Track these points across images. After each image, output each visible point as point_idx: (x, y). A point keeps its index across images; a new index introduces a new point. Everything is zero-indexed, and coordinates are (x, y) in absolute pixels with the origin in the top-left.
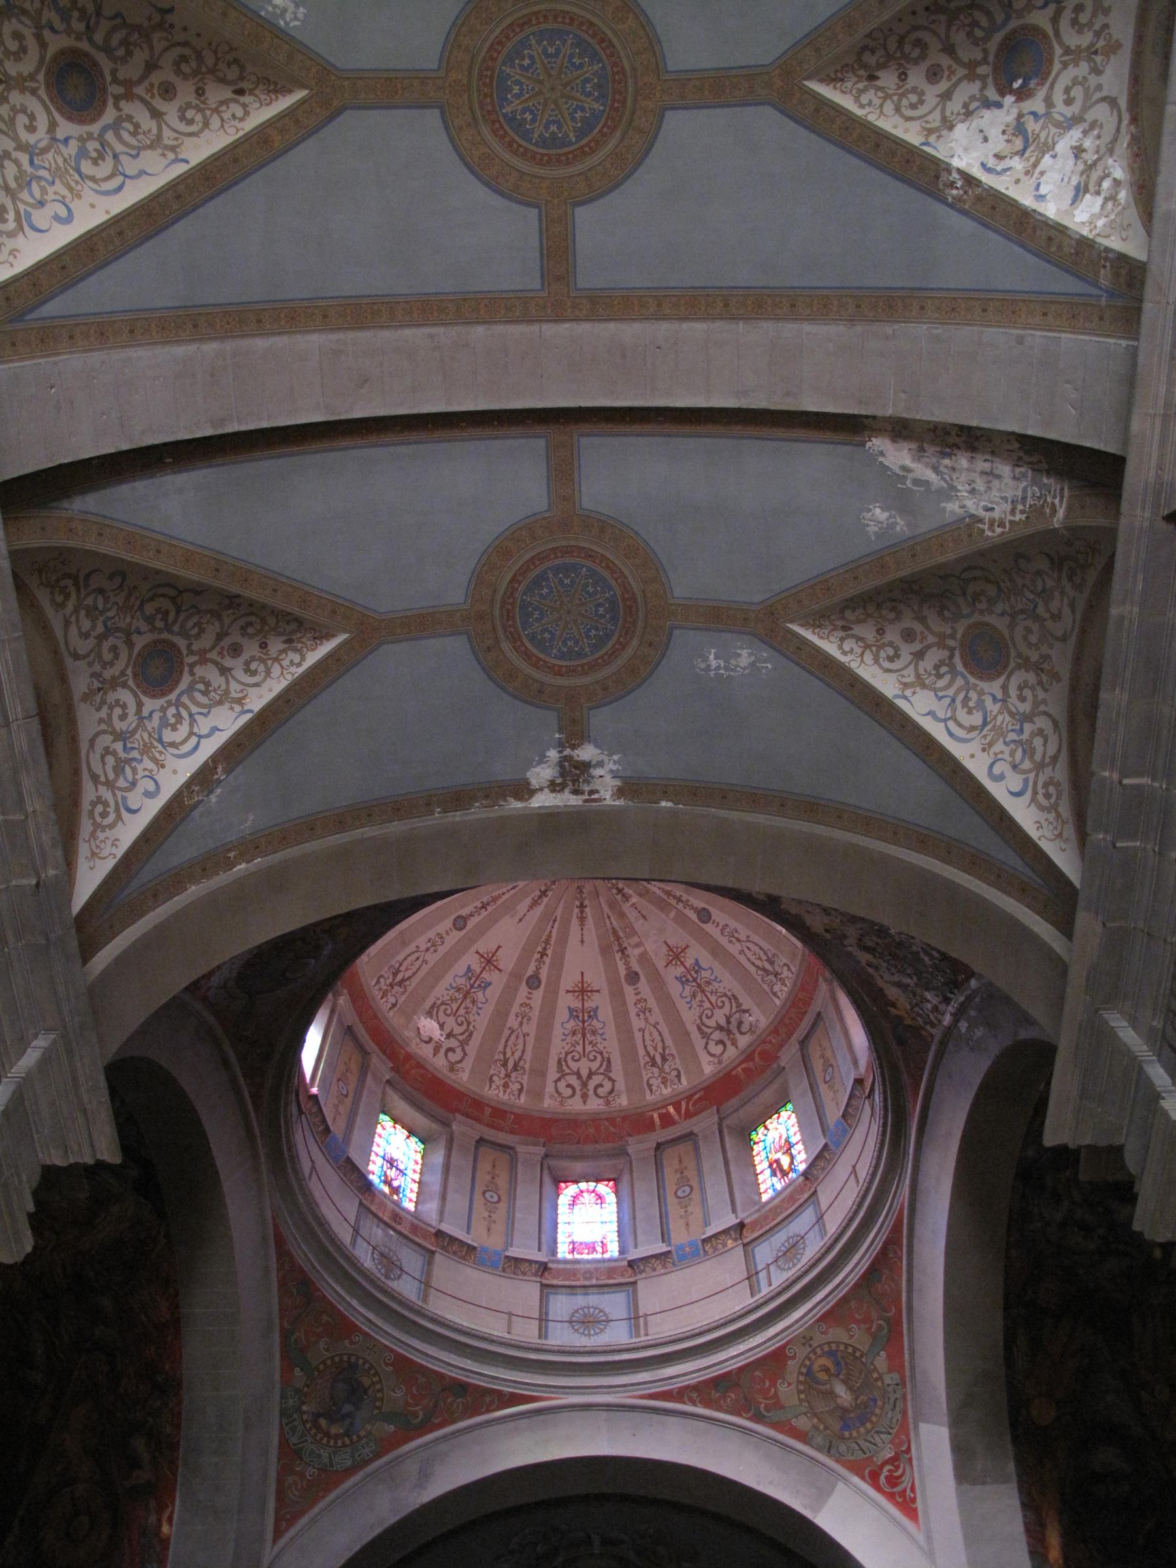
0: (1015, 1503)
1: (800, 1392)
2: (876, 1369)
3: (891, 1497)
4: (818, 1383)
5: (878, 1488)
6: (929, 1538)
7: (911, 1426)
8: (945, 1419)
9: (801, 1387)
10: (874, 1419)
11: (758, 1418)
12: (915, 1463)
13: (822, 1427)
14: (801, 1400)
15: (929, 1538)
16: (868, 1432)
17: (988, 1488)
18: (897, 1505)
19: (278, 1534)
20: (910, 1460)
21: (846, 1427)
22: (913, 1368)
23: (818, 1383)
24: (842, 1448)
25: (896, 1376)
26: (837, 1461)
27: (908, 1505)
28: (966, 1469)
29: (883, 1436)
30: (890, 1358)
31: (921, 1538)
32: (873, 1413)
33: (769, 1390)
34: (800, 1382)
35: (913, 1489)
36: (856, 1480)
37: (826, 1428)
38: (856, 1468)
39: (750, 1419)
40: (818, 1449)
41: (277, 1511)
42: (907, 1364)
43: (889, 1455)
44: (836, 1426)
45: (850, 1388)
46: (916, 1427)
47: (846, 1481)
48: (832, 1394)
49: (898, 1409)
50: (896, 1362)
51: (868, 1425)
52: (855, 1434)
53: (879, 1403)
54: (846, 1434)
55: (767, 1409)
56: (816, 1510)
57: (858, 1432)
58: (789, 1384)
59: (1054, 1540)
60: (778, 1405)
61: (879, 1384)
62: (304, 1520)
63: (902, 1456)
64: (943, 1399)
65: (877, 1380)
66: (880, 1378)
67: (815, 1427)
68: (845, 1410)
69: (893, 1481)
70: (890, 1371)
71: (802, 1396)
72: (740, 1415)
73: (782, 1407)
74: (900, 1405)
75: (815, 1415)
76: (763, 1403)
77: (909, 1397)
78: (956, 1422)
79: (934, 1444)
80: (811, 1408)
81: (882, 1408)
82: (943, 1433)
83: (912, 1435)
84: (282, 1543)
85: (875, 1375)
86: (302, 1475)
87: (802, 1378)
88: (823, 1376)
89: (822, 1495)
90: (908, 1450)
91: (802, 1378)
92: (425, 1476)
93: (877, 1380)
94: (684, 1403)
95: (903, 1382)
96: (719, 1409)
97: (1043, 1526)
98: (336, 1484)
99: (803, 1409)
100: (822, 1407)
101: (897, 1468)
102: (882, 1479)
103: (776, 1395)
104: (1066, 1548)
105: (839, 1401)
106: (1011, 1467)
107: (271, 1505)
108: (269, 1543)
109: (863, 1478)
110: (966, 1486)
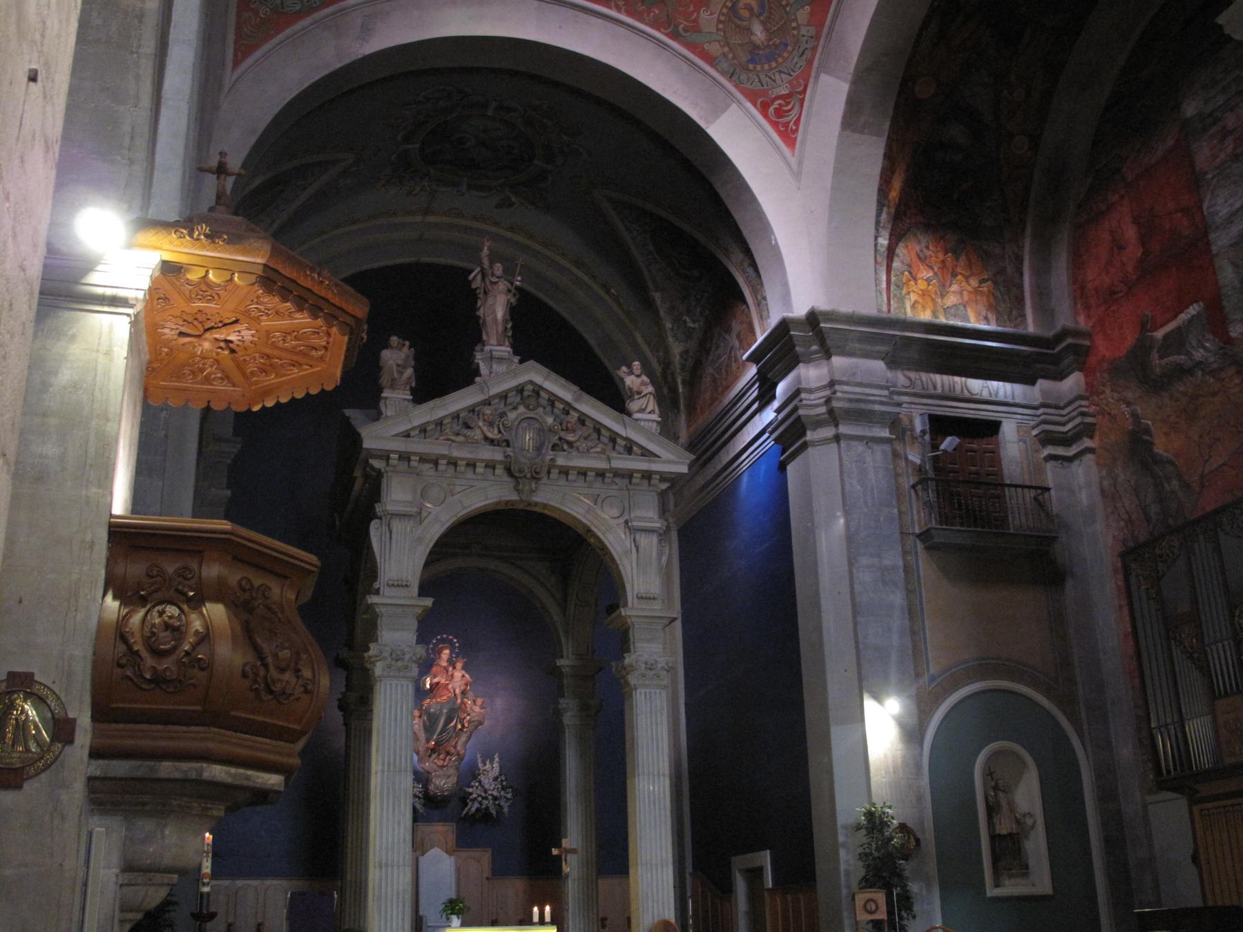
0: (881, 151)
1: (719, 21)
2: (796, 19)
3: (775, 125)
4: (741, 19)
5: (766, 116)
6: (800, 163)
7: (813, 74)
8: (850, 77)
9: (722, 18)
10: (780, 60)
11: (674, 36)
12: (806, 104)
13: (730, 56)
14: (718, 30)
15: (800, 163)
16: (771, 69)
17: (864, 137)
18: (780, 133)
19: (236, 63)
20: (802, 101)
21: (752, 61)
22: (831, 28)
23: (741, 19)
24: (743, 77)
25: (812, 30)
26: (736, 86)
27: (788, 135)
28: (852, 119)
29: (783, 76)
30: (812, 14)
31: (793, 161)
32: (780, 55)
33: (691, 14)
34: (721, 13)
35: (797, 122)
36: (749, 105)
37: (734, 58)
38: (752, 96)
39: (667, 35)
40: (723, 73)
41: (236, 42)
42: (828, 22)
43: (784, 92)
44: (744, 57)
45: (766, 30)
46: (817, 77)
47: (739, 102)
48: (749, 30)
49: (804, 57)
50: (817, 20)
51: (774, 64)
52: (759, 68)
53: (790, 48)
54: (751, 66)
55: (685, 30)
56: (708, 123)
57: (762, 68)
58: (712, 14)
59: (897, 184)
60: (696, 29)
61: (795, 32)
62: (258, 54)
63: (798, 94)
64: (855, 58)
65: (794, 28)
66: (797, 28)
67: (724, 55)
68: (756, 47)
69: (780, 113)
70: (809, 25)
71: (721, 26)
72: (658, 29)
73: (699, 31)
74: (808, 54)
75: (728, 44)
76: (683, 23)
77: (820, 49)
78: (858, 80)
79: (829, 96)
80: (725, 37)
81: (790, 53)
82: (844, 88)
83: (811, 80)
84: (243, 66)
85: (794, 25)
86: (257, 13)
87: (725, 11)
88: (746, 14)
89: (717, 112)
90: (804, 91)
91: (725, 11)
92: (366, 31)
93: (794, 28)
94: (610, 8)
95: (817, 37)
96: (641, 20)
97: (893, 172)
98: (289, 24)
99: (719, 38)
100: (735, 40)
101: (788, 103)
102: (771, 109)
103: (695, 21)
104: (903, 190)
105: (753, 38)
106: (887, 125)
107: (231, 37)
108: (229, 65)
109: (755, 105)
110: (847, 133)
